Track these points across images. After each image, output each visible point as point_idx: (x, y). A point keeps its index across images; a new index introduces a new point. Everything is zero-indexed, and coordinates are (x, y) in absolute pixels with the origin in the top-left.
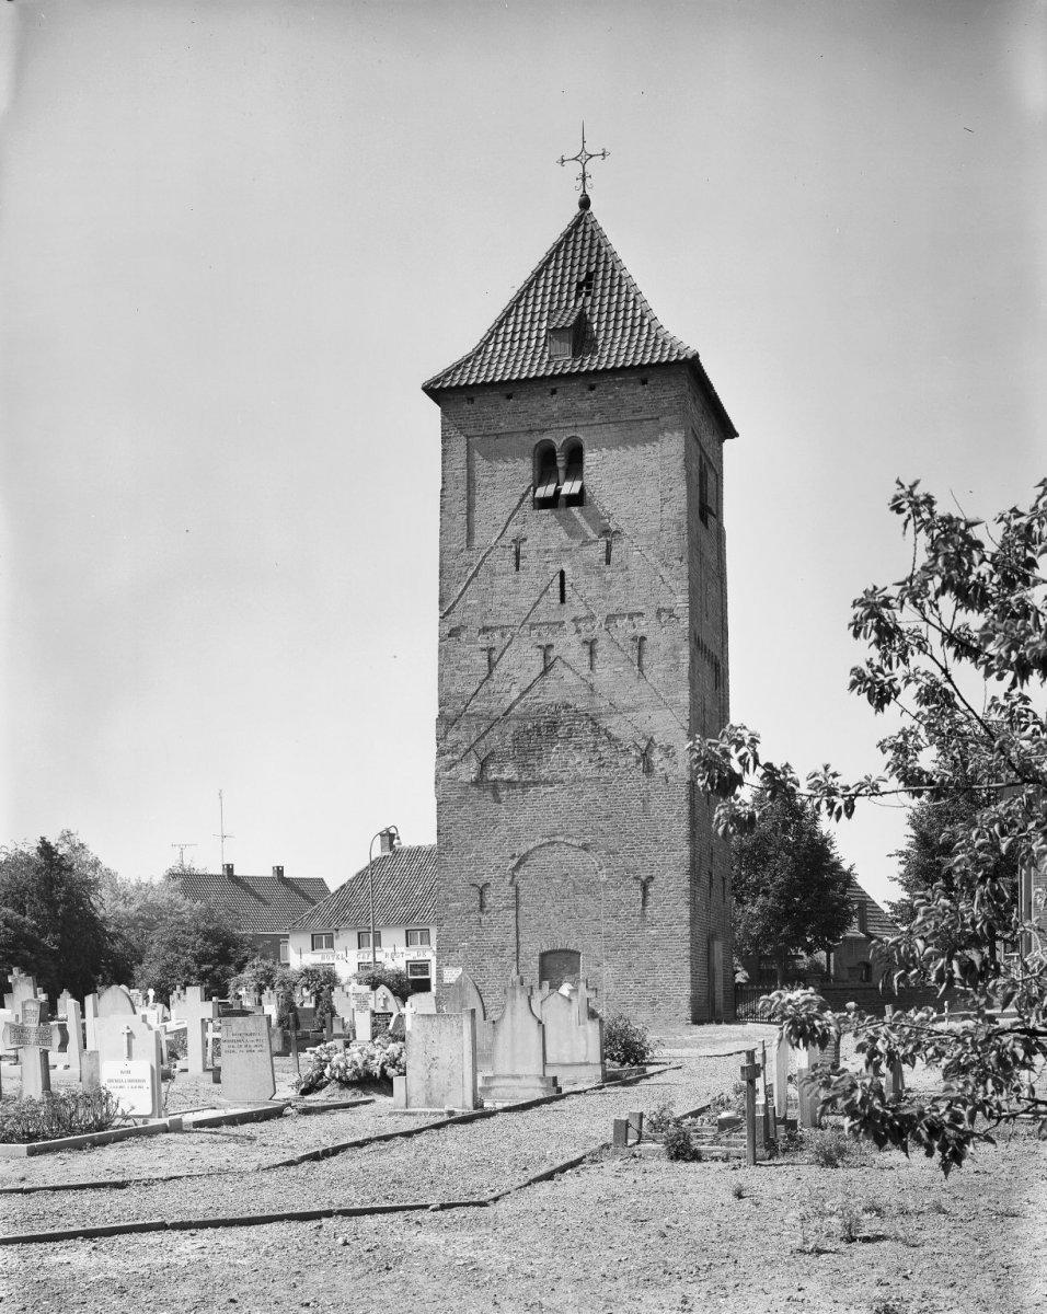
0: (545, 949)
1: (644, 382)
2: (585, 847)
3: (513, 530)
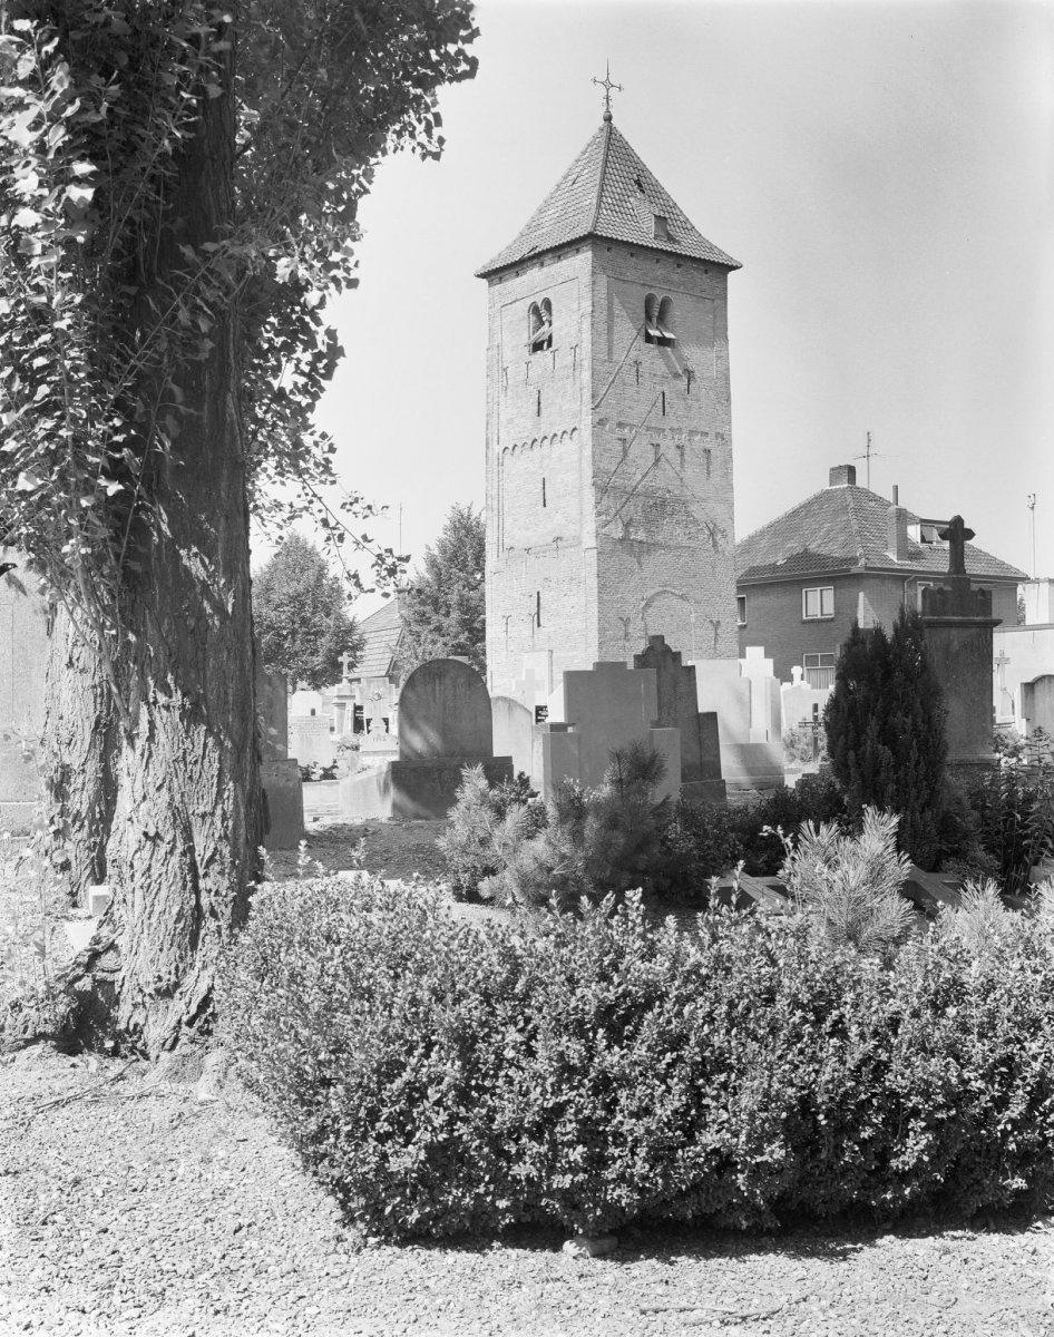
1: (706, 272)
2: (682, 597)
3: (633, 354)
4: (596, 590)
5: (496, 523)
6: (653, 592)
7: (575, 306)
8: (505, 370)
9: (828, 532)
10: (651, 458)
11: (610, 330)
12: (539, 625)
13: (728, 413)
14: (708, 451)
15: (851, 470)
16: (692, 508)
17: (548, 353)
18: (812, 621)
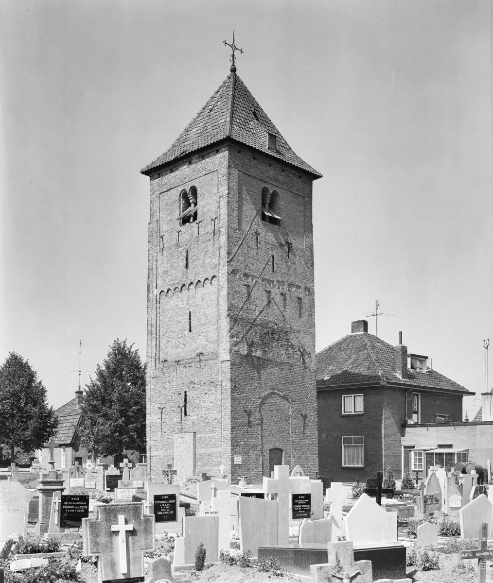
0: (271, 447)
1: (300, 177)
2: (284, 397)
3: (254, 227)
4: (229, 391)
5: (154, 343)
6: (266, 393)
7: (215, 190)
8: (162, 237)
9: (356, 360)
10: (265, 299)
11: (240, 208)
12: (186, 414)
13: (312, 274)
14: (300, 299)
15: (365, 324)
16: (291, 336)
17: (194, 224)
18: (349, 416)
